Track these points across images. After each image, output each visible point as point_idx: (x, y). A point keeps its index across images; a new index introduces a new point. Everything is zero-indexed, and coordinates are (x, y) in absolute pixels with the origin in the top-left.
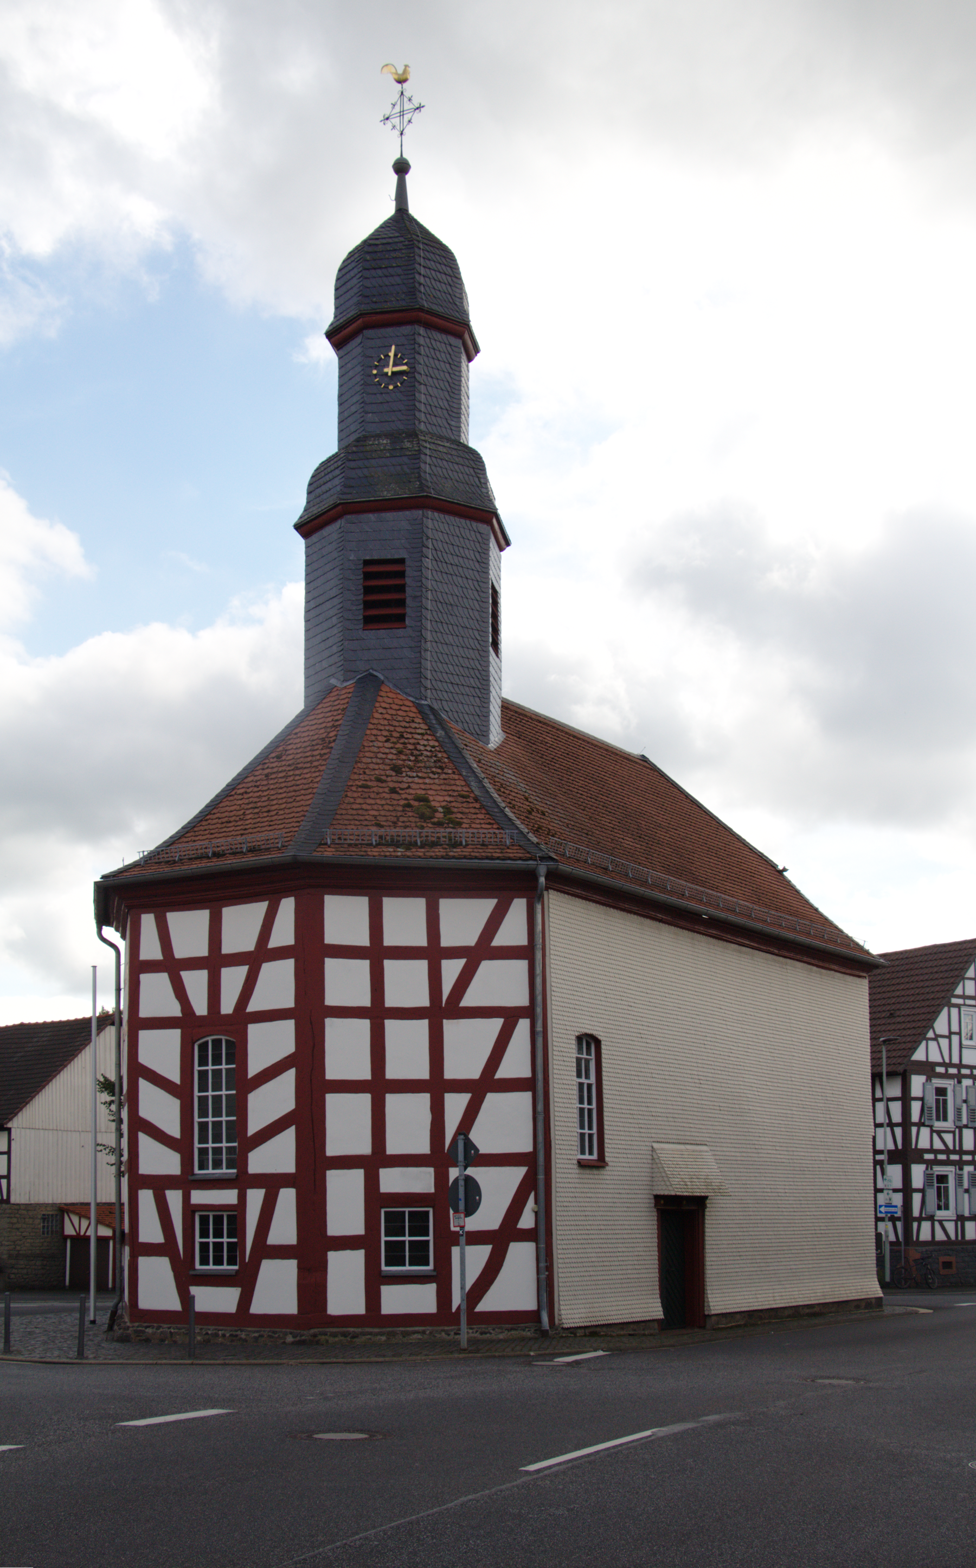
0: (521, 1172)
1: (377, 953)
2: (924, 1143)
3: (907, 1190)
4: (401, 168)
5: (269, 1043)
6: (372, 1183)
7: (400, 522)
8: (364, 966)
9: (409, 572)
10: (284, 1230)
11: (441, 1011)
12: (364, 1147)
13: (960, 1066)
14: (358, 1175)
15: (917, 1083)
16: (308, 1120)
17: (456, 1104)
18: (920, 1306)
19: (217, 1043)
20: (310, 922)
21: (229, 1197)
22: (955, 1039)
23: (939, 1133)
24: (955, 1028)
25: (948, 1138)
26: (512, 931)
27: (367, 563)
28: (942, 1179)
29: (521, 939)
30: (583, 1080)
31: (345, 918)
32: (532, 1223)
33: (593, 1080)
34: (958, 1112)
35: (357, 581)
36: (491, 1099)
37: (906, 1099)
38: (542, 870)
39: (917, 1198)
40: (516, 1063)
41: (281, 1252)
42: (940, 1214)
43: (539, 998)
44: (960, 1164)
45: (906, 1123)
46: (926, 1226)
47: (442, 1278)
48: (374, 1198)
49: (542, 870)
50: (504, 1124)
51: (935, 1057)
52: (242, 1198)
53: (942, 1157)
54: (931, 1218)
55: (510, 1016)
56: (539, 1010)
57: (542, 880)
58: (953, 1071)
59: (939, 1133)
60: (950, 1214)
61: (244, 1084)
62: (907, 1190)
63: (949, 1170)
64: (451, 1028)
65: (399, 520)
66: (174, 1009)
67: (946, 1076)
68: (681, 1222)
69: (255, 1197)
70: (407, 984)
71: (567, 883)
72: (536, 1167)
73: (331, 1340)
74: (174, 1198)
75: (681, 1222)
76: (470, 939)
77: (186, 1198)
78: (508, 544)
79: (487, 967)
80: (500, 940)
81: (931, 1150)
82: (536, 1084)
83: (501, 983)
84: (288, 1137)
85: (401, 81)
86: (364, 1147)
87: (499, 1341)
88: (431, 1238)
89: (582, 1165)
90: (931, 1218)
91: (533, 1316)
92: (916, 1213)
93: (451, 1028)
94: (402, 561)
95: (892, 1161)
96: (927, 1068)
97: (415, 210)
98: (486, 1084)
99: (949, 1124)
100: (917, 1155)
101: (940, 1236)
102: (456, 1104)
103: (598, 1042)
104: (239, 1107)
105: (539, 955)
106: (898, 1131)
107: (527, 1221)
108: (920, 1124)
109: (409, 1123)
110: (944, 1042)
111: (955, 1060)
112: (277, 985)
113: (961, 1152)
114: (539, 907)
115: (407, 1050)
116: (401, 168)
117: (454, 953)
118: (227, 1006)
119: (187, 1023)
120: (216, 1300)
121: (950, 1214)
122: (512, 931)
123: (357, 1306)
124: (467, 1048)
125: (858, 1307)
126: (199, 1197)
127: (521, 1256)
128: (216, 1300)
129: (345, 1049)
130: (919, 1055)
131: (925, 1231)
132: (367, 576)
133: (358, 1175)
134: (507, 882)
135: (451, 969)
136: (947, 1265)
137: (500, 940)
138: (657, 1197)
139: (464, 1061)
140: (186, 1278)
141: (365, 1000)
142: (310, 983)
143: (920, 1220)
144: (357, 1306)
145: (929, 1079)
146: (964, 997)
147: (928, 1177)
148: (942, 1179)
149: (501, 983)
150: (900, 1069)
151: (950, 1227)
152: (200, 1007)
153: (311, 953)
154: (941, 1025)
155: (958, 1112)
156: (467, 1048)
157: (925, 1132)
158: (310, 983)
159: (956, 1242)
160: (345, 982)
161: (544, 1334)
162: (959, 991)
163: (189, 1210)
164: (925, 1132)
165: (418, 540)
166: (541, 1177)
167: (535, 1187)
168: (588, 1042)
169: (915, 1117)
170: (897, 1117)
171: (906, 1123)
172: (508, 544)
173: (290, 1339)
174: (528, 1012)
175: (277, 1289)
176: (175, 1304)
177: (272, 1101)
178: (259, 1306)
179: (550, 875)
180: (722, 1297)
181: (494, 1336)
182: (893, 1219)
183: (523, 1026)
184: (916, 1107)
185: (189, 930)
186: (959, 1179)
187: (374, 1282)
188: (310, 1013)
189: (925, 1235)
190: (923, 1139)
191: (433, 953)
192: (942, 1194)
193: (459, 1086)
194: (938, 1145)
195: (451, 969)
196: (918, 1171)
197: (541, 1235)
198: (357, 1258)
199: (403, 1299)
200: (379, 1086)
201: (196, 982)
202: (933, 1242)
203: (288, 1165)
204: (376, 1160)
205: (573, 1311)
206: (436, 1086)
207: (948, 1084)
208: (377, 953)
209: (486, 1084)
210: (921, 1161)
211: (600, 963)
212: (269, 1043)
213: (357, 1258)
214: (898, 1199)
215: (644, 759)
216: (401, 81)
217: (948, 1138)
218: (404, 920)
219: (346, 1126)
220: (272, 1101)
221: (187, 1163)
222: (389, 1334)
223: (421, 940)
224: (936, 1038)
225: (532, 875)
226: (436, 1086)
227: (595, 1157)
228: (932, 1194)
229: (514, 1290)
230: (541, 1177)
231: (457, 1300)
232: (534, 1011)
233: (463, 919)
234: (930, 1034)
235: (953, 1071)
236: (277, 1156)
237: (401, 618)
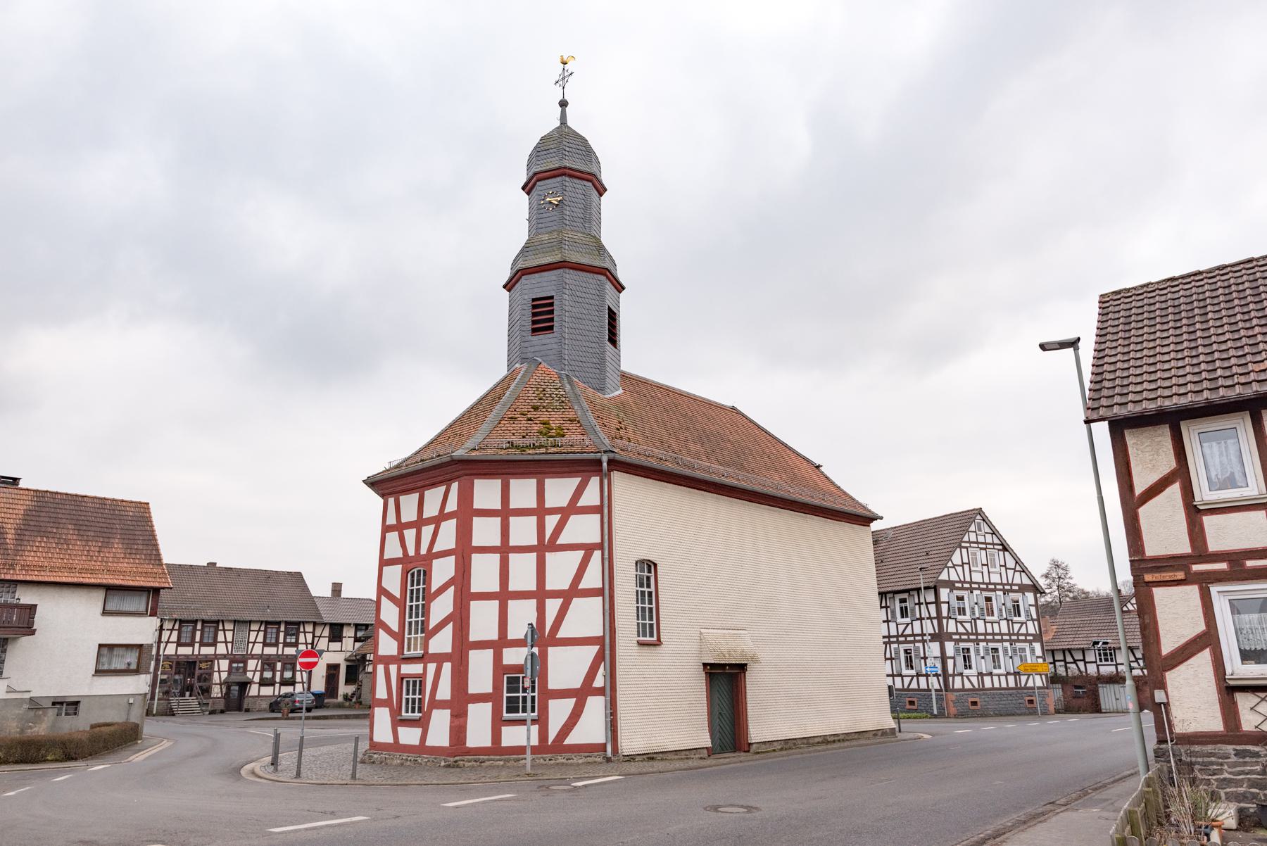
0: (594, 649)
1: (505, 513)
2: (952, 628)
3: (944, 658)
4: (563, 104)
5: (443, 570)
6: (498, 658)
7: (562, 282)
8: (497, 521)
9: (556, 303)
10: (444, 692)
11: (544, 547)
12: (494, 635)
13: (971, 582)
14: (489, 654)
15: (944, 593)
16: (460, 619)
17: (553, 606)
18: (920, 730)
19: (419, 572)
20: (466, 497)
21: (416, 669)
22: (966, 567)
23: (961, 623)
24: (965, 560)
25: (968, 626)
26: (591, 496)
27: (534, 300)
28: (996, 650)
29: (596, 501)
30: (645, 589)
31: (486, 493)
32: (602, 682)
33: (653, 589)
34: (973, 610)
35: (528, 312)
36: (576, 602)
37: (937, 602)
38: (605, 459)
39: (950, 663)
40: (592, 579)
41: (442, 705)
42: (967, 672)
43: (606, 537)
44: (977, 642)
45: (939, 617)
46: (958, 679)
47: (542, 721)
48: (499, 668)
49: (605, 459)
50: (585, 618)
51: (954, 577)
52: (425, 669)
53: (1022, 638)
54: (961, 674)
55: (588, 549)
56: (606, 545)
57: (605, 464)
58: (966, 586)
59: (961, 623)
60: (974, 671)
61: (429, 597)
62: (944, 658)
63: (971, 645)
64: (550, 557)
65: (552, 275)
66: (399, 553)
67: (962, 588)
68: (726, 679)
69: (432, 667)
70: (524, 531)
71: (616, 465)
72: (605, 648)
73: (467, 764)
74: (393, 669)
75: (726, 679)
76: (564, 502)
77: (399, 669)
78: (623, 288)
79: (573, 519)
80: (582, 502)
81: (957, 633)
82: (606, 592)
83: (584, 529)
84: (448, 630)
85: (565, 63)
86: (494, 635)
87: (578, 765)
88: (505, 695)
89: (641, 644)
90: (961, 674)
91: (603, 747)
92: (951, 672)
93: (550, 557)
94: (552, 297)
95: (1034, 640)
96: (950, 585)
97: (571, 123)
98: (573, 592)
99: (967, 617)
100: (949, 637)
101: (968, 685)
102: (553, 606)
103: (655, 565)
104: (426, 611)
105: (606, 511)
106: (935, 622)
107: (599, 682)
108: (949, 618)
109: (522, 616)
110: (959, 569)
111: (986, 580)
112: (448, 536)
113: (977, 634)
114: (606, 482)
115: (523, 573)
116: (563, 104)
117: (553, 511)
118: (423, 551)
119: (404, 560)
120: (410, 736)
121: (974, 671)
122: (591, 496)
123: (487, 742)
124: (561, 570)
125: (875, 735)
126: (408, 669)
127: (595, 707)
128: (410, 736)
129: (484, 573)
130: (944, 576)
131: (958, 683)
132: (534, 307)
133: (489, 654)
134: (585, 467)
135: (551, 522)
136: (974, 703)
137: (582, 502)
138: (705, 665)
139: (559, 578)
140: (398, 722)
141: (497, 542)
142: (464, 533)
143: (954, 675)
144: (487, 742)
145: (951, 591)
146: (969, 542)
147: (957, 650)
148: (996, 650)
149: (584, 529)
150: (932, 585)
151: (974, 680)
152: (411, 552)
153: (466, 514)
154: (956, 559)
155: (973, 610)
156: (561, 570)
157: (952, 622)
158: (464, 533)
159: (979, 690)
160: (485, 532)
161: (608, 760)
162: (966, 539)
163: (401, 678)
164: (952, 622)
165: (562, 286)
166: (607, 652)
167: (603, 659)
168: (648, 567)
169: (945, 613)
170: (934, 614)
171: (939, 617)
172: (623, 288)
173: (443, 764)
174: (600, 546)
175: (439, 731)
176: (390, 740)
177: (442, 607)
178: (430, 742)
179: (610, 462)
180: (761, 728)
181: (575, 761)
182: (937, 675)
183: (597, 555)
184: (944, 607)
185: (409, 504)
186: (1005, 649)
187: (498, 723)
188: (464, 551)
189: (958, 685)
190: (952, 627)
191: (541, 512)
192: (967, 659)
193: (555, 594)
194: (961, 630)
195: (551, 522)
196: (950, 647)
197: (610, 692)
198: (487, 707)
199: (514, 736)
200: (504, 596)
201: (410, 534)
202: (963, 689)
203: (448, 649)
204: (501, 643)
205: (631, 743)
206: (541, 594)
207: (965, 594)
208: (505, 513)
209: (573, 592)
210: (951, 639)
211: (647, 517)
212: (443, 570)
213: (487, 707)
214: (939, 665)
215: (734, 408)
216: (565, 63)
217: (968, 626)
218: (523, 492)
219: (483, 620)
220: (442, 607)
221: (401, 648)
222: (505, 760)
223: (533, 504)
224: (954, 566)
225: (599, 462)
226: (541, 594)
227: (655, 638)
228: (960, 660)
229: (591, 729)
230: (607, 652)
231: (552, 735)
232: (605, 545)
233: (559, 490)
234: (950, 564)
235: (966, 586)
236: (442, 642)
237: (551, 328)
